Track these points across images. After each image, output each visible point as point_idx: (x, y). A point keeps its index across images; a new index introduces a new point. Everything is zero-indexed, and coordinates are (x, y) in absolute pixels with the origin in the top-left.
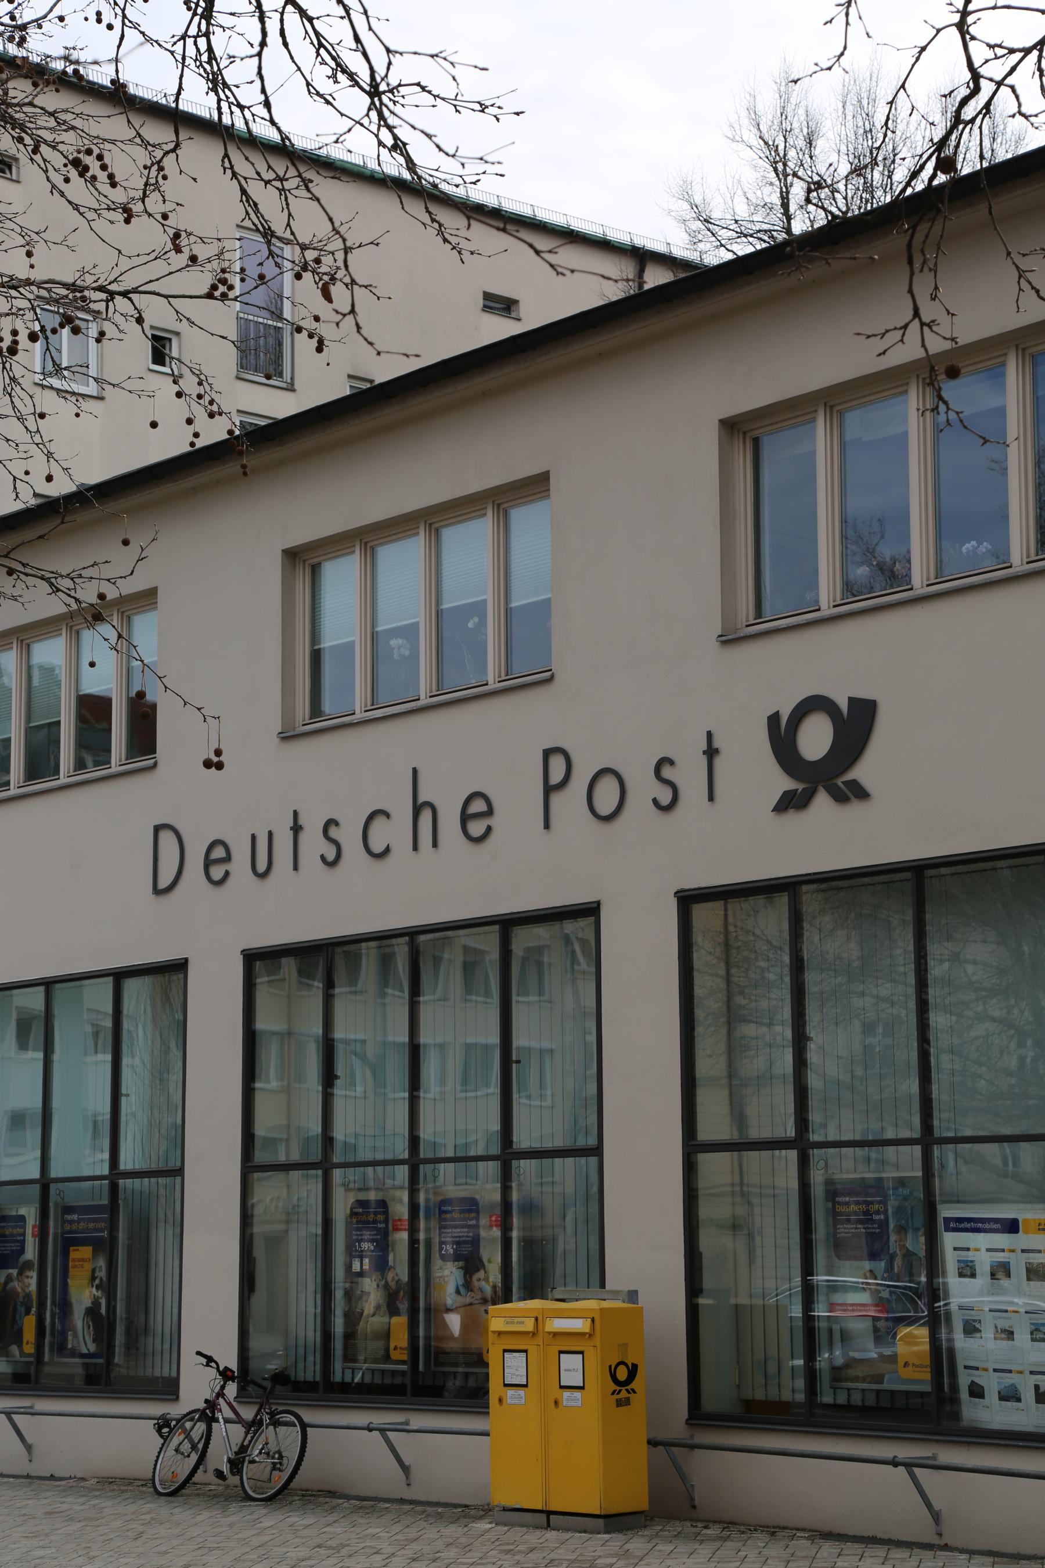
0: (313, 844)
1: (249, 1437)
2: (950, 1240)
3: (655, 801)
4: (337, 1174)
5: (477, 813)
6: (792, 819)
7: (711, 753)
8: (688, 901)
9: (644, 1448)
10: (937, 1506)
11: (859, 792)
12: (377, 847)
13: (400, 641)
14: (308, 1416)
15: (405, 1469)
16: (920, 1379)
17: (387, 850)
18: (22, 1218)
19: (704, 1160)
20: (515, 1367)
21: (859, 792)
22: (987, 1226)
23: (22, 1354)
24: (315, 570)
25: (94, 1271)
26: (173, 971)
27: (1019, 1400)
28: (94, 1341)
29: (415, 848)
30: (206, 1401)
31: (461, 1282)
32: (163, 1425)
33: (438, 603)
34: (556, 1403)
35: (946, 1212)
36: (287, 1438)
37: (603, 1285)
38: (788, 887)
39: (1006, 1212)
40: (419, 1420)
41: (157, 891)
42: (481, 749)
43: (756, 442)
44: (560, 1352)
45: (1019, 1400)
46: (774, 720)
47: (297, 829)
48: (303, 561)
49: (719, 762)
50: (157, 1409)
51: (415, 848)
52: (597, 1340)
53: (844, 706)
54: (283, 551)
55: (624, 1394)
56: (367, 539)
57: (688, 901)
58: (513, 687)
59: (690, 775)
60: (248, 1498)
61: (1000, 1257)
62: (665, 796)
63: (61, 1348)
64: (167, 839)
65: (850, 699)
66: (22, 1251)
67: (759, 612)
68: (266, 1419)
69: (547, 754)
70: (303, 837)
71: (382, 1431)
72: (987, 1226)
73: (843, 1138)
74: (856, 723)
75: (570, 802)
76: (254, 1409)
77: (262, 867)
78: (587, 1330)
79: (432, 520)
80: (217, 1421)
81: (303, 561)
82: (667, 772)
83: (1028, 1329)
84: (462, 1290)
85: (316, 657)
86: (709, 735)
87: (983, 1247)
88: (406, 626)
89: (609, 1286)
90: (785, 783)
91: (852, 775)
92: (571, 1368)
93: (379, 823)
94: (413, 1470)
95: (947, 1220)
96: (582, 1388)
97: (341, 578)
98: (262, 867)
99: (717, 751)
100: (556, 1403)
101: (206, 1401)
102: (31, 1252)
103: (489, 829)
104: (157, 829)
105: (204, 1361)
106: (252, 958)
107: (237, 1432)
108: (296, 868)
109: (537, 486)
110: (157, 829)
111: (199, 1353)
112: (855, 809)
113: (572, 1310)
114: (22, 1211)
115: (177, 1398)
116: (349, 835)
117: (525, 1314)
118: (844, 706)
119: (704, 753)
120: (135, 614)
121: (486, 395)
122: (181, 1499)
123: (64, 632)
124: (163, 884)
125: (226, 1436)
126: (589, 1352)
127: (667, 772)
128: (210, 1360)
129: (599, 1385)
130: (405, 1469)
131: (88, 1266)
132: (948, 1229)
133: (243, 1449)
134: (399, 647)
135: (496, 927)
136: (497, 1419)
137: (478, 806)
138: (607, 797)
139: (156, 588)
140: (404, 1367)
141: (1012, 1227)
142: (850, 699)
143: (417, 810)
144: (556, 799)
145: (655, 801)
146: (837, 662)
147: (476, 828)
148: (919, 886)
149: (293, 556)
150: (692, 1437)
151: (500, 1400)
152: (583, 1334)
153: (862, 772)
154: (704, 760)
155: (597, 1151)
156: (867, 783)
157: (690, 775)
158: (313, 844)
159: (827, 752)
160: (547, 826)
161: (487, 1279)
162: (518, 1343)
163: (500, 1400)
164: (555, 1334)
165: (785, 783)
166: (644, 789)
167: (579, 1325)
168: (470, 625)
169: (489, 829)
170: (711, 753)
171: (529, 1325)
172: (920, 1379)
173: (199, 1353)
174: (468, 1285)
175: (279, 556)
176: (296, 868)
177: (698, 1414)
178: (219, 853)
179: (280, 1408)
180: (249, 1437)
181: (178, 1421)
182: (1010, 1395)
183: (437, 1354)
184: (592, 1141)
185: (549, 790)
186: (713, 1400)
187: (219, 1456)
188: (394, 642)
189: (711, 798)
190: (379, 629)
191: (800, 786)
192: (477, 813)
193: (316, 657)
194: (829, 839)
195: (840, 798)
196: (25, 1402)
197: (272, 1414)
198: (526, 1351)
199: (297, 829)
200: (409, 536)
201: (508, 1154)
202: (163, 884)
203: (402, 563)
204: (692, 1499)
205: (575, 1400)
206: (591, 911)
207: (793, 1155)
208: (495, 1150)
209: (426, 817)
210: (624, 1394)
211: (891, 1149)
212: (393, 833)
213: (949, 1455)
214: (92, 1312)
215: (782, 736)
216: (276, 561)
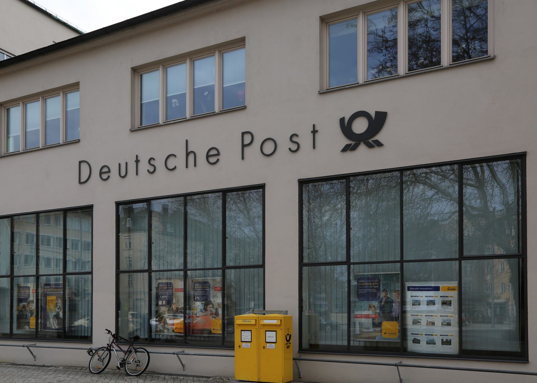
0: (144, 166)
1: (126, 356)
2: (409, 294)
3: (148, 170)
5: (213, 155)
7: (314, 132)
11: (379, 144)
12: (171, 166)
13: (176, 100)
14: (149, 349)
15: (183, 365)
17: (175, 168)
18: (29, 287)
20: (246, 336)
21: (379, 144)
22: (428, 289)
23: (30, 328)
24: (8, 110)
25: (57, 304)
28: (57, 325)
29: (187, 167)
30: (108, 344)
31: (202, 308)
32: (90, 351)
33: (46, 119)
36: (142, 357)
37: (264, 309)
38: (346, 178)
39: (433, 284)
40: (187, 351)
41: (80, 183)
42: (222, 132)
43: (141, 76)
46: (342, 120)
47: (137, 161)
48: (138, 72)
49: (317, 135)
50: (88, 346)
51: (187, 167)
52: (282, 327)
53: (373, 115)
55: (288, 344)
57: (118, 204)
58: (67, 143)
59: (305, 140)
60: (128, 375)
61: (431, 299)
63: (45, 326)
65: (376, 112)
66: (29, 296)
69: (243, 134)
70: (140, 164)
72: (426, 289)
73: (390, 260)
74: (378, 121)
75: (253, 151)
76: (128, 347)
77: (123, 174)
78: (279, 323)
79: (44, 95)
80: (113, 350)
81: (138, 72)
82: (152, 162)
83: (426, 322)
84: (203, 311)
86: (137, 156)
87: (423, 296)
88: (180, 94)
89: (266, 309)
91: (376, 138)
92: (271, 336)
93: (171, 160)
94: (185, 366)
95: (409, 288)
98: (123, 174)
99: (139, 161)
101: (108, 344)
102: (31, 298)
103: (109, 177)
105: (107, 332)
106: (302, 183)
109: (75, 87)
110: (80, 162)
111: (106, 330)
112: (377, 150)
114: (29, 285)
116: (159, 163)
117: (251, 318)
118: (373, 115)
119: (312, 132)
120: (144, 73)
124: (83, 180)
125: (117, 356)
126: (279, 331)
127: (152, 162)
128: (109, 332)
129: (282, 341)
130: (183, 365)
131: (55, 302)
132: (408, 290)
133: (124, 360)
134: (175, 102)
136: (237, 351)
137: (105, 170)
138: (269, 148)
139: (79, 82)
140: (182, 334)
141: (437, 289)
142: (376, 112)
143: (188, 154)
144: (246, 149)
145: (148, 170)
146: (372, 100)
147: (105, 176)
150: (300, 356)
153: (380, 137)
154: (135, 163)
157: (305, 140)
158: (144, 166)
161: (213, 307)
162: (246, 328)
164: (264, 325)
165: (346, 141)
166: (284, 144)
167: (275, 322)
168: (205, 94)
169: (109, 177)
171: (253, 322)
173: (106, 330)
174: (205, 309)
176: (137, 174)
177: (301, 350)
179: (138, 347)
180: (126, 356)
181: (96, 351)
183: (193, 330)
184: (90, 270)
185: (244, 146)
186: (305, 345)
188: (173, 101)
191: (353, 143)
192: (213, 155)
193: (141, 104)
194: (364, 160)
196: (33, 343)
199: (137, 161)
200: (57, 96)
203: (34, 110)
205: (248, 345)
206: (262, 187)
207: (146, 274)
208: (182, 267)
209: (191, 157)
210: (288, 344)
212: (179, 161)
214: (57, 316)
215: (346, 127)
216: (317, 22)
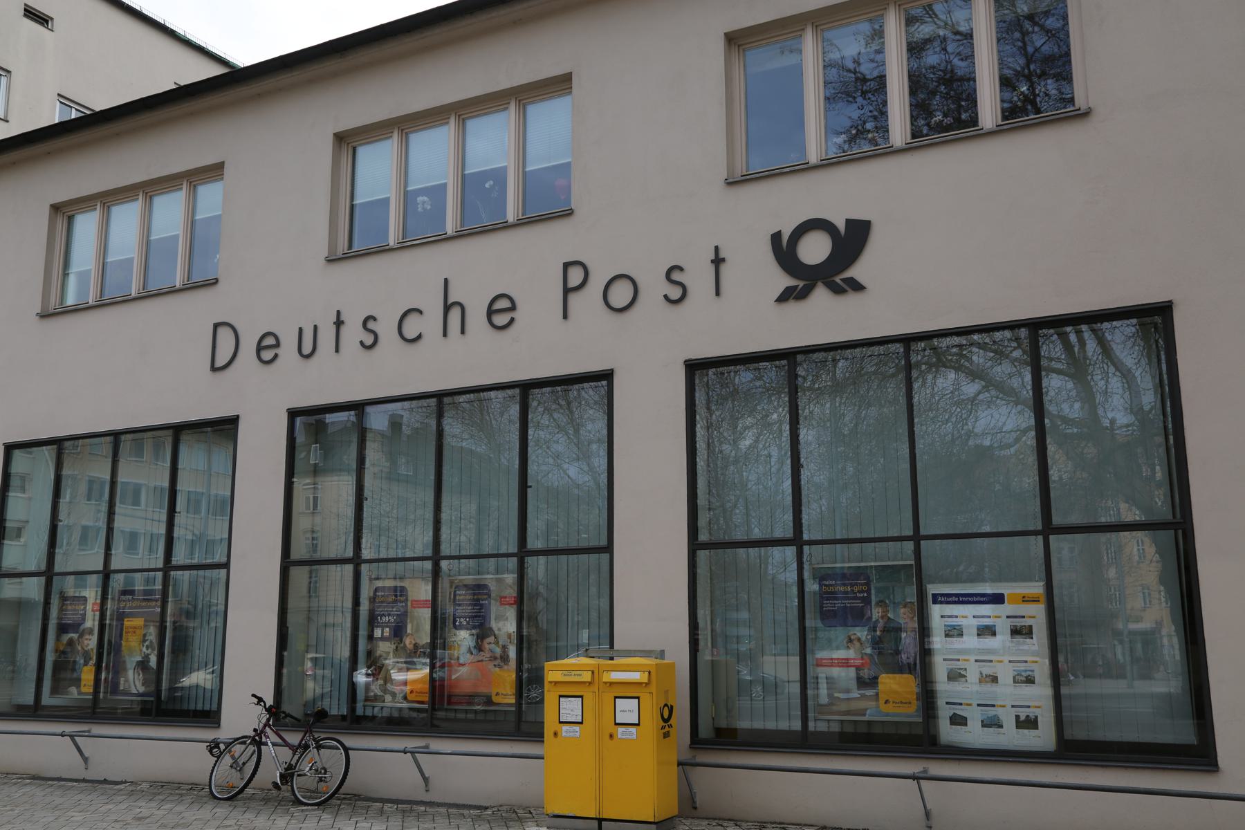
0: (353, 333)
1: (296, 757)
3: (361, 343)
4: (364, 568)
5: (501, 311)
6: (792, 307)
7: (718, 261)
8: (293, 414)
9: (675, 768)
10: (928, 807)
11: (856, 286)
13: (426, 199)
14: (349, 741)
15: (426, 779)
16: (910, 712)
17: (420, 337)
18: (85, 599)
19: (530, 560)
20: (571, 709)
21: (856, 286)
22: (979, 599)
24: (70, 219)
25: (145, 635)
26: (226, 428)
27: (1001, 726)
30: (255, 730)
31: (472, 644)
32: (213, 746)
33: (148, 236)
34: (611, 736)
35: (932, 589)
36: (332, 759)
37: (612, 646)
38: (789, 355)
39: (988, 589)
41: (214, 369)
42: (520, 263)
43: (354, 149)
44: (616, 697)
45: (1001, 726)
46: (776, 237)
47: (339, 323)
48: (347, 142)
50: (209, 734)
52: (653, 688)
53: (841, 226)
54: (335, 134)
56: (107, 199)
57: (293, 414)
59: (698, 278)
62: (369, 340)
64: (224, 333)
67: (350, 247)
68: (312, 744)
69: (566, 266)
71: (412, 753)
74: (852, 239)
75: (587, 302)
76: (300, 736)
78: (589, 679)
80: (266, 744)
81: (64, 212)
82: (371, 325)
84: (474, 651)
85: (352, 207)
86: (338, 312)
87: (968, 615)
90: (785, 281)
91: (848, 274)
92: (627, 710)
95: (935, 596)
96: (638, 725)
97: (86, 225)
99: (723, 260)
100: (611, 736)
101: (255, 730)
104: (216, 326)
105: (256, 700)
107: (286, 754)
108: (337, 350)
109: (561, 84)
110: (216, 326)
111: (254, 695)
113: (628, 665)
115: (219, 726)
116: (387, 328)
117: (582, 668)
118: (841, 226)
121: (311, 82)
122: (240, 803)
123: (184, 186)
124: (218, 364)
125: (275, 757)
126: (645, 698)
127: (371, 325)
128: (260, 700)
129: (652, 721)
130: (426, 779)
131: (140, 632)
132: (935, 602)
134: (424, 202)
135: (517, 391)
136: (550, 746)
139: (223, 163)
140: (426, 706)
141: (998, 599)
143: (447, 308)
144: (573, 299)
145: (361, 343)
146: (840, 195)
148: (911, 352)
149: (341, 139)
150: (694, 757)
151: (555, 734)
152: (640, 684)
153: (857, 271)
155: (608, 549)
156: (861, 279)
157: (698, 278)
158: (353, 333)
159: (829, 259)
160: (565, 316)
161: (497, 643)
162: (571, 690)
163: (555, 734)
164: (611, 684)
165: (785, 281)
166: (654, 288)
167: (635, 676)
168: (487, 185)
169: (276, 356)
170: (718, 261)
171: (587, 677)
172: (910, 712)
173: (254, 695)
174: (479, 648)
175: (331, 137)
177: (696, 741)
178: (270, 341)
179: (323, 736)
182: (992, 723)
183: (450, 696)
184: (604, 542)
185: (567, 291)
186: (705, 731)
187: (271, 771)
188: (420, 199)
189: (718, 293)
190: (409, 189)
191: (801, 284)
192: (501, 311)
193: (352, 207)
194: (823, 319)
195: (837, 290)
197: (317, 742)
198: (581, 697)
199: (339, 323)
201: (917, 538)
202: (218, 364)
203: (126, 218)
204: (694, 802)
205: (631, 733)
206: (606, 376)
209: (455, 315)
211: (741, 551)
212: (429, 323)
213: (937, 768)
214: (143, 665)
215: (784, 252)
